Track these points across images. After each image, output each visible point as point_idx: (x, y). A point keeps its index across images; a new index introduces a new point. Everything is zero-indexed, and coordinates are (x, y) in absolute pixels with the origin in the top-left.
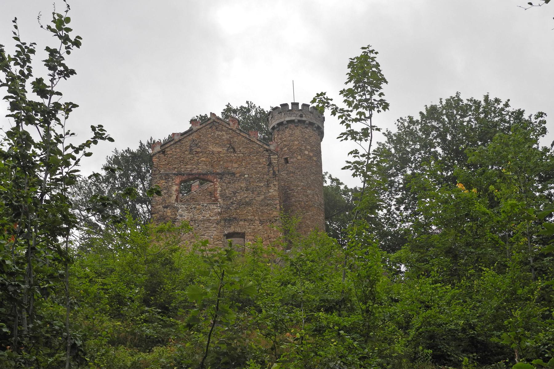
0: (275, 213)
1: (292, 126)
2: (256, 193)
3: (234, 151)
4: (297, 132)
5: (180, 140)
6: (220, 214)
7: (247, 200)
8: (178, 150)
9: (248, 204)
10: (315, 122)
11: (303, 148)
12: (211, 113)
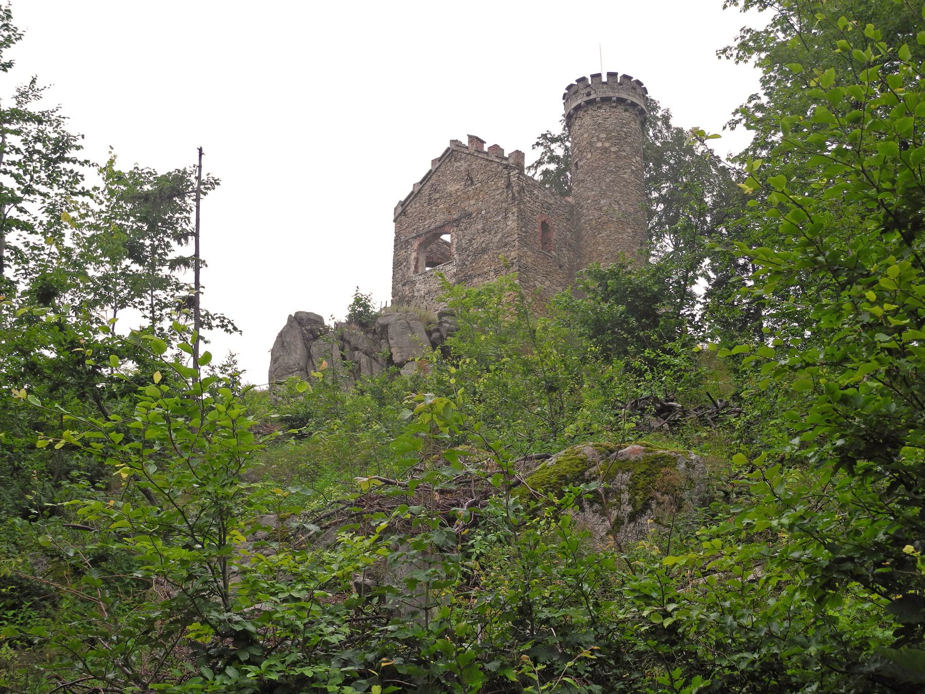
0: (513, 253)
1: (581, 113)
2: (493, 232)
3: (472, 183)
4: (587, 120)
5: (420, 190)
6: (455, 275)
7: (484, 245)
8: (418, 205)
9: (484, 251)
10: (611, 94)
11: (595, 139)
12: (470, 137)
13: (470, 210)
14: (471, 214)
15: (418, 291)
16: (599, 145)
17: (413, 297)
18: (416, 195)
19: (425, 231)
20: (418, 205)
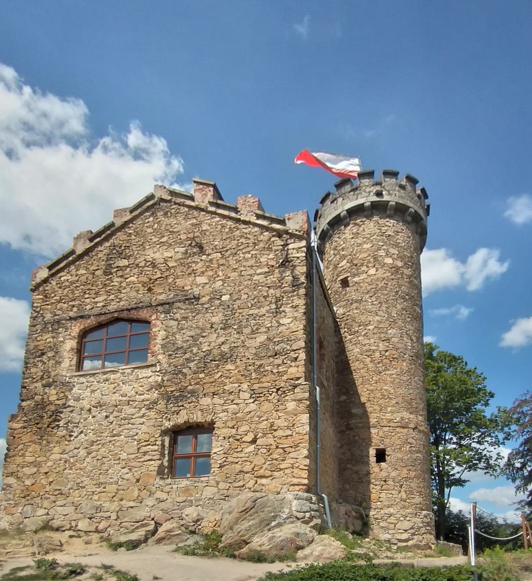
2: (247, 331)
7: (225, 348)
9: (224, 358)
13: (196, 291)
14: (197, 299)
15: (77, 399)
16: (389, 261)
17: (65, 406)
18: (80, 257)
19: (96, 311)
20: (82, 271)
